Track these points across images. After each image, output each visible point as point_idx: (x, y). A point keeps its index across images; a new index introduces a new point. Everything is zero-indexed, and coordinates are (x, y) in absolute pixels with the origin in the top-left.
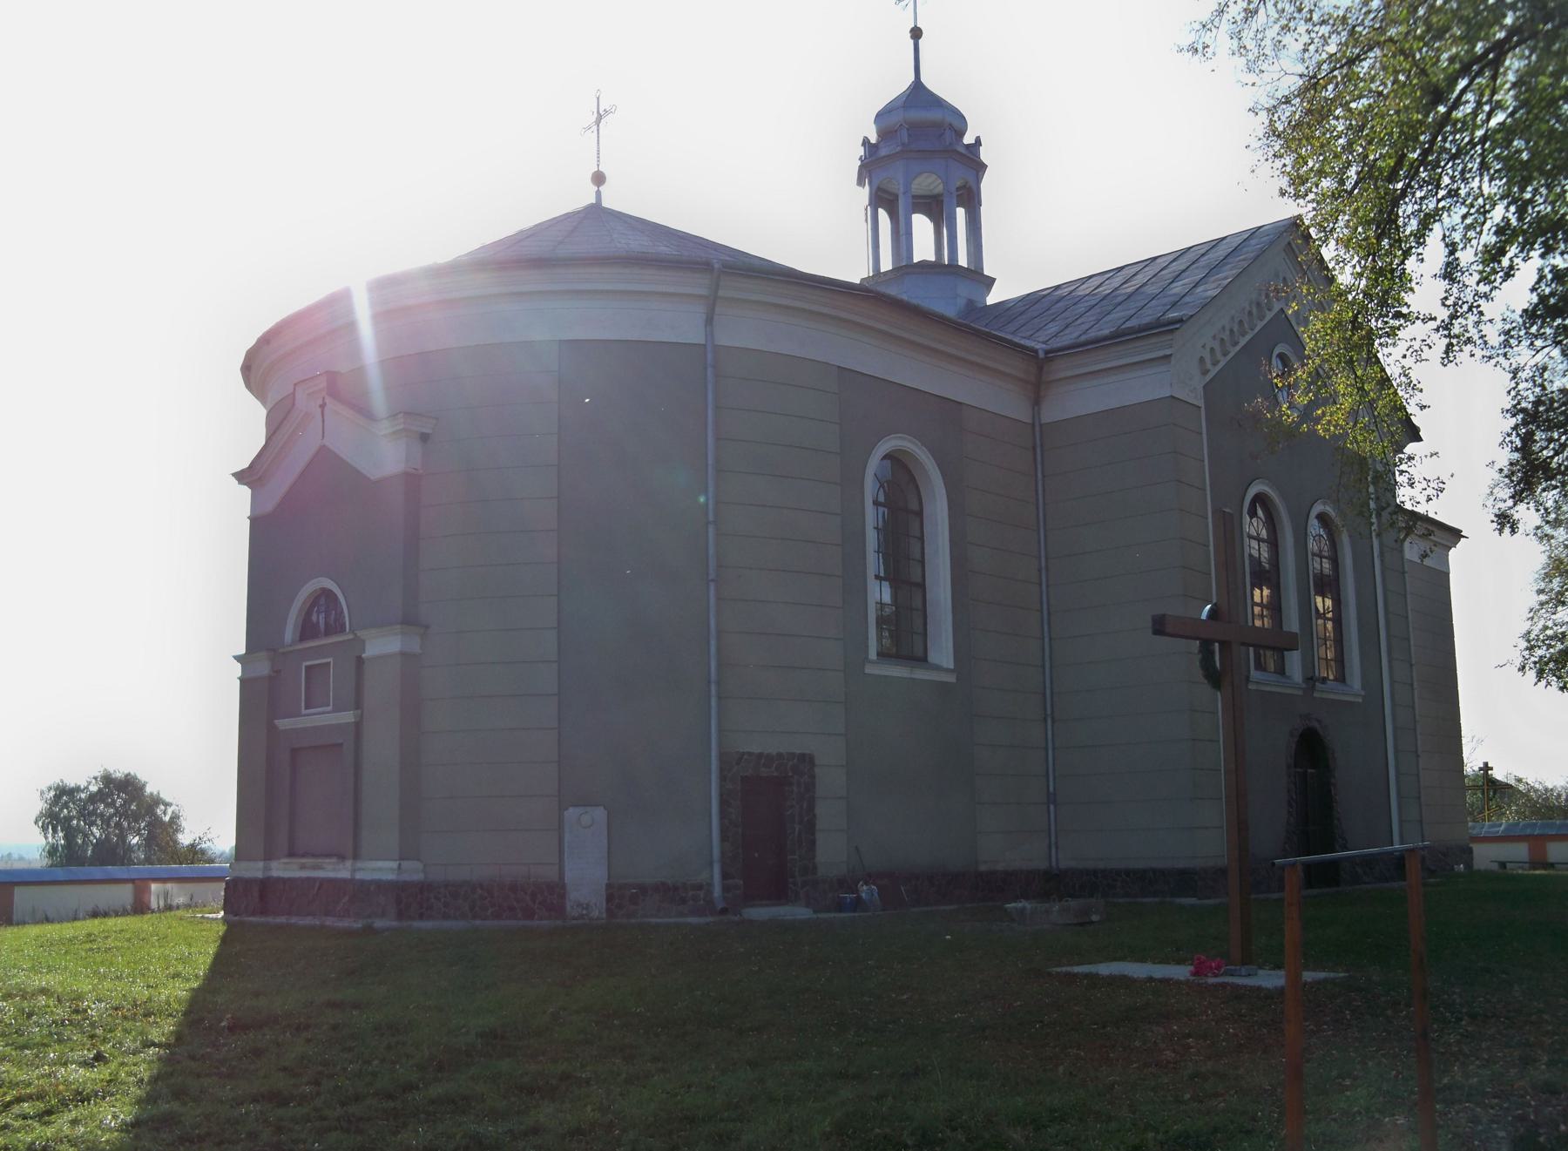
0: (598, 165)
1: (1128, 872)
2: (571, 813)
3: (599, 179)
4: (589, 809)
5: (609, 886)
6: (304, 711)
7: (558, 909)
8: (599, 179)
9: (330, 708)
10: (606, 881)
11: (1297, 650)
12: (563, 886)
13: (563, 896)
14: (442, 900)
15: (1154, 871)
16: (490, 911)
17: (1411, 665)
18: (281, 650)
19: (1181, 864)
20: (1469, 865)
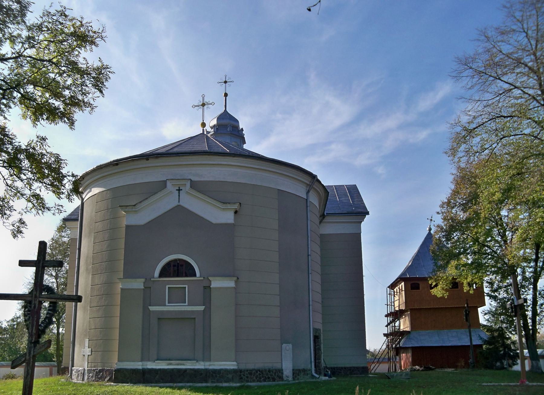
0: (203, 121)
1: (345, 368)
2: (284, 345)
3: (432, 217)
4: (288, 344)
5: (293, 370)
6: (167, 304)
7: (281, 378)
8: (432, 217)
9: (187, 304)
10: (292, 369)
11: (419, 284)
12: (282, 370)
13: (282, 373)
14: (246, 375)
15: (354, 367)
16: (262, 379)
17: (308, 255)
18: (152, 279)
19: (362, 365)
20: (49, 353)
